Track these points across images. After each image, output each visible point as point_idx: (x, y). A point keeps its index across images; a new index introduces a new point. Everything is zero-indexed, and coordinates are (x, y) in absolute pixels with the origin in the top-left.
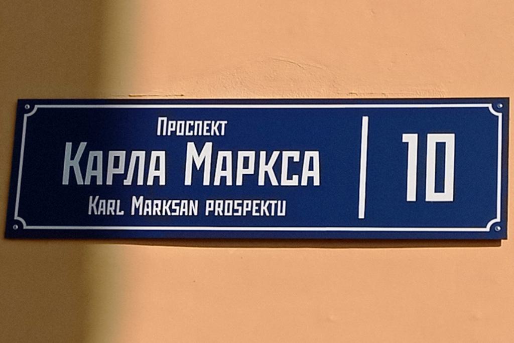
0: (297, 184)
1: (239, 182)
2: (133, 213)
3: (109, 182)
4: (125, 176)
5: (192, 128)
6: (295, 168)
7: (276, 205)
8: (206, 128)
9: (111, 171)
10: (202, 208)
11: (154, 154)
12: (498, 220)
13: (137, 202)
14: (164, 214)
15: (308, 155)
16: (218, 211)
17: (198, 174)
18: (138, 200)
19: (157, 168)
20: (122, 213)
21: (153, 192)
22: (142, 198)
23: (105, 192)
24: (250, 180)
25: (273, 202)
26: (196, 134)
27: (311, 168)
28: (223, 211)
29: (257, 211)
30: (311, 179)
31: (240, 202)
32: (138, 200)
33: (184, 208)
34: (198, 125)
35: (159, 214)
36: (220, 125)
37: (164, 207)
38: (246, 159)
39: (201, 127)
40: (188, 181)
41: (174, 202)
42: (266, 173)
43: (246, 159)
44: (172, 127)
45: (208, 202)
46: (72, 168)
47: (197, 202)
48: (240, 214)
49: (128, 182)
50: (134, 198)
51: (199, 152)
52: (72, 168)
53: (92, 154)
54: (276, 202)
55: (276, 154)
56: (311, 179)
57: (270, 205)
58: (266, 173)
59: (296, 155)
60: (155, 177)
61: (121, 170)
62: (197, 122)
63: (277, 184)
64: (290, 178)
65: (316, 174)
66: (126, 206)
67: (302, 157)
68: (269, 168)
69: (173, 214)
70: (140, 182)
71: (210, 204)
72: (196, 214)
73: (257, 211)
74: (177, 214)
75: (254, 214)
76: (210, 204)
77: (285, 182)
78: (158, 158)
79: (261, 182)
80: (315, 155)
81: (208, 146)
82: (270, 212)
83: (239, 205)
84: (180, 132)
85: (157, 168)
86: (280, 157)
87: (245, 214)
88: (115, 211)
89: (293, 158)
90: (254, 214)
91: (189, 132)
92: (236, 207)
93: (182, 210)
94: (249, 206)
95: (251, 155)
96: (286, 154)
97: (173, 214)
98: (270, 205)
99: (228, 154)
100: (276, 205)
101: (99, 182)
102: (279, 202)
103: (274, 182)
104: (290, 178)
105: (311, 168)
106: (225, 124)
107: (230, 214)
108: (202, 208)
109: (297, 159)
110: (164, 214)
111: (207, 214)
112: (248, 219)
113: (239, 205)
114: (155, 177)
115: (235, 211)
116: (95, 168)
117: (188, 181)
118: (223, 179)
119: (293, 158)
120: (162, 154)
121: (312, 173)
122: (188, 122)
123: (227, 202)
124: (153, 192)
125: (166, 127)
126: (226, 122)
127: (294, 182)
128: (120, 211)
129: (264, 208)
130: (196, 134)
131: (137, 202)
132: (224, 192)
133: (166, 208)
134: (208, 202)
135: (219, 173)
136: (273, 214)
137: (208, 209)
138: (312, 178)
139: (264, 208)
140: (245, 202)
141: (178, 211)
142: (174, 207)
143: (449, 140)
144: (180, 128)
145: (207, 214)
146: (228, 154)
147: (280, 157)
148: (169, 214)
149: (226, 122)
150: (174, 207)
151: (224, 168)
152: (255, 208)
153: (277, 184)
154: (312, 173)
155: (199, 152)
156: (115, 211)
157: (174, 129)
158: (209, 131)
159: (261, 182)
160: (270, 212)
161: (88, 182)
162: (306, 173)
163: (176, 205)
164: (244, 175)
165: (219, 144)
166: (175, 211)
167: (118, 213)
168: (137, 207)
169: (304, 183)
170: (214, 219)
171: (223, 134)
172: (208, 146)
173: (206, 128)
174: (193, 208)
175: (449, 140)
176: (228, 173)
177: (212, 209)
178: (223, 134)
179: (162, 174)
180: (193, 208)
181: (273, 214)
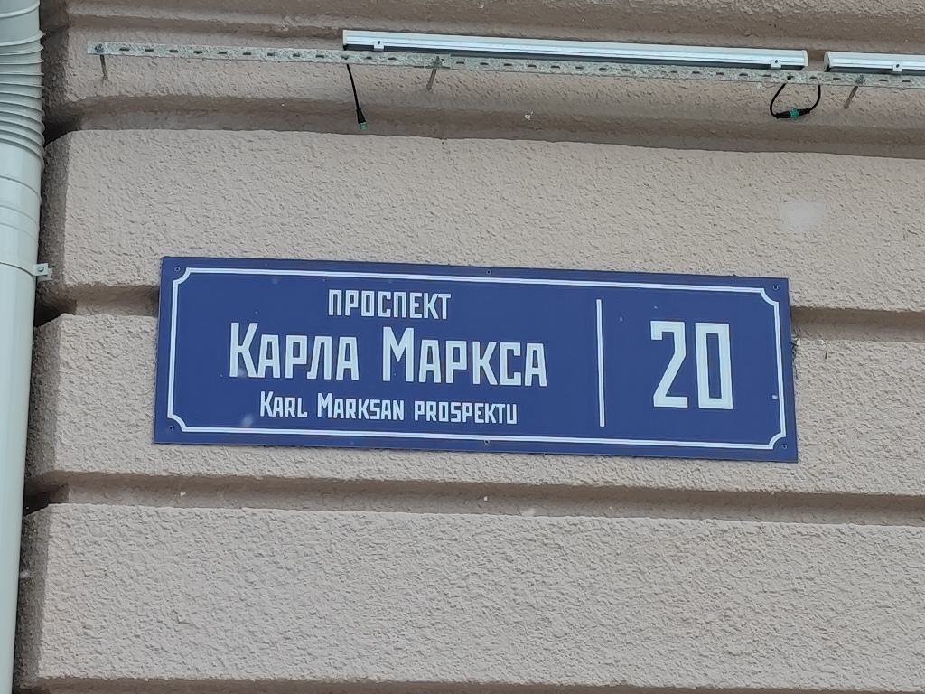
0: (520, 384)
1: (450, 380)
2: (319, 416)
3: (289, 374)
4: (308, 367)
5: (388, 304)
6: (516, 364)
7: (504, 410)
8: (414, 305)
9: (291, 361)
10: (409, 410)
11: (344, 341)
12: (783, 434)
13: (324, 401)
14: (360, 417)
15: (531, 347)
16: (431, 415)
17: (398, 366)
18: (325, 398)
19: (348, 358)
20: (305, 415)
21: (342, 389)
22: (330, 395)
23: (281, 387)
24: (463, 376)
25: (501, 406)
26: (396, 315)
27: (535, 365)
28: (437, 416)
29: (480, 417)
30: (536, 378)
31: (458, 404)
32: (325, 398)
33: (386, 410)
34: (400, 298)
35: (354, 417)
36: (439, 300)
37: (360, 409)
38: (456, 351)
39: (405, 303)
40: (387, 376)
41: (373, 402)
42: (482, 368)
43: (456, 351)
44: (352, 301)
45: (417, 403)
46: (240, 356)
47: (402, 402)
48: (458, 420)
49: (312, 375)
50: (320, 395)
51: (398, 340)
52: (240, 356)
53: (265, 339)
54: (504, 406)
55: (492, 346)
56: (536, 378)
57: (497, 409)
58: (482, 368)
59: (516, 348)
60: (428, 372)
61: (302, 360)
62: (397, 295)
63: (496, 383)
64: (510, 376)
65: (541, 371)
66: (310, 405)
67: (524, 350)
68: (485, 363)
69: (372, 418)
70: (328, 376)
71: (420, 406)
72: (402, 418)
73: (480, 417)
74: (377, 417)
75: (477, 420)
76: (420, 406)
77: (505, 381)
78: (270, 344)
79: (476, 380)
80: (540, 348)
81: (409, 334)
82: (497, 419)
83: (456, 408)
84: (368, 310)
85: (348, 358)
86: (497, 350)
87: (465, 420)
88: (296, 412)
89: (513, 350)
90: (477, 420)
91: (384, 311)
92: (453, 411)
93: (384, 413)
94: (468, 410)
95: (462, 345)
96: (505, 347)
97: (372, 418)
98: (497, 409)
99: (434, 344)
100: (504, 410)
101: (276, 374)
102: (508, 406)
103: (492, 381)
104: (510, 376)
105: (535, 365)
106: (448, 299)
107: (446, 420)
108: (409, 410)
109: (517, 353)
110: (360, 417)
111: (416, 419)
112: (471, 426)
113: (456, 408)
114: (428, 372)
115: (452, 416)
116: (269, 356)
117: (387, 376)
118: (430, 374)
119: (513, 350)
120: (352, 341)
121: (537, 372)
122: (381, 294)
123: (441, 404)
124: (342, 389)
125: (340, 303)
126: (449, 296)
127: (516, 380)
128: (302, 413)
129: (489, 413)
130: (396, 315)
131: (324, 401)
132: (431, 390)
133: (362, 409)
134: (417, 403)
135: (424, 367)
136: (501, 421)
137: (417, 413)
138: (350, 370)
139: (489, 413)
140: (465, 405)
141: (378, 413)
142: (372, 409)
143: (722, 330)
144: (367, 304)
145: (416, 419)
146: (434, 344)
147: (497, 350)
148: (367, 417)
149: (449, 296)
150: (372, 409)
151: (430, 361)
152: (478, 413)
153: (496, 383)
154: (537, 372)
155: (398, 340)
156: (296, 412)
157: (355, 305)
158: (419, 310)
159: (476, 380)
160: (497, 419)
161: (262, 374)
162: (530, 371)
163: (376, 405)
164: (454, 370)
165: (425, 329)
166: (375, 413)
167: (300, 415)
168: (325, 407)
169: (528, 382)
170: (424, 425)
171: (444, 317)
172: (409, 334)
173: (414, 305)
174: (399, 410)
175: (722, 330)
176: (435, 367)
177: (422, 412)
178: (444, 317)
179: (354, 365)
180: (399, 410)
181: (501, 421)
